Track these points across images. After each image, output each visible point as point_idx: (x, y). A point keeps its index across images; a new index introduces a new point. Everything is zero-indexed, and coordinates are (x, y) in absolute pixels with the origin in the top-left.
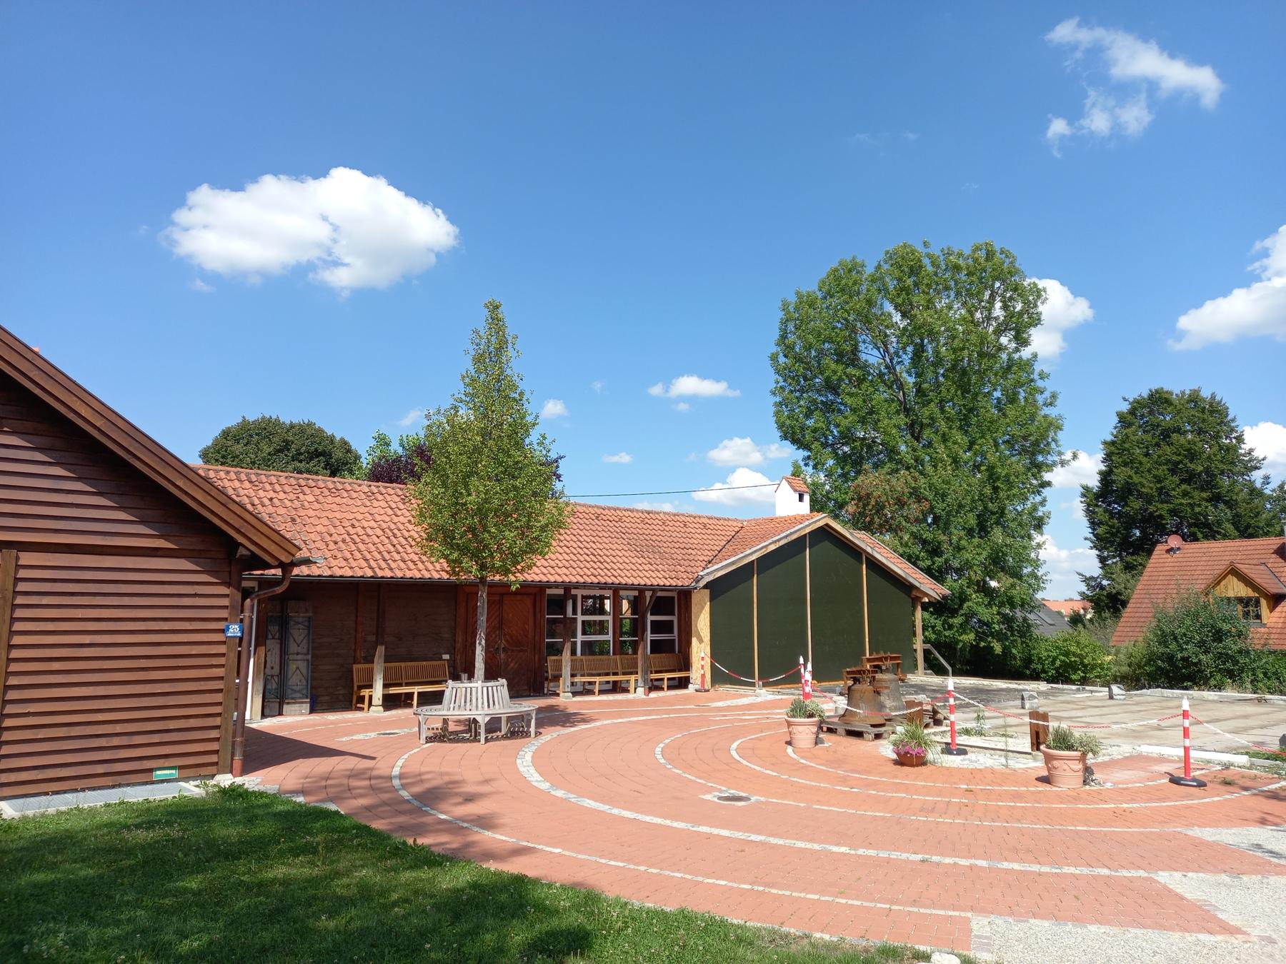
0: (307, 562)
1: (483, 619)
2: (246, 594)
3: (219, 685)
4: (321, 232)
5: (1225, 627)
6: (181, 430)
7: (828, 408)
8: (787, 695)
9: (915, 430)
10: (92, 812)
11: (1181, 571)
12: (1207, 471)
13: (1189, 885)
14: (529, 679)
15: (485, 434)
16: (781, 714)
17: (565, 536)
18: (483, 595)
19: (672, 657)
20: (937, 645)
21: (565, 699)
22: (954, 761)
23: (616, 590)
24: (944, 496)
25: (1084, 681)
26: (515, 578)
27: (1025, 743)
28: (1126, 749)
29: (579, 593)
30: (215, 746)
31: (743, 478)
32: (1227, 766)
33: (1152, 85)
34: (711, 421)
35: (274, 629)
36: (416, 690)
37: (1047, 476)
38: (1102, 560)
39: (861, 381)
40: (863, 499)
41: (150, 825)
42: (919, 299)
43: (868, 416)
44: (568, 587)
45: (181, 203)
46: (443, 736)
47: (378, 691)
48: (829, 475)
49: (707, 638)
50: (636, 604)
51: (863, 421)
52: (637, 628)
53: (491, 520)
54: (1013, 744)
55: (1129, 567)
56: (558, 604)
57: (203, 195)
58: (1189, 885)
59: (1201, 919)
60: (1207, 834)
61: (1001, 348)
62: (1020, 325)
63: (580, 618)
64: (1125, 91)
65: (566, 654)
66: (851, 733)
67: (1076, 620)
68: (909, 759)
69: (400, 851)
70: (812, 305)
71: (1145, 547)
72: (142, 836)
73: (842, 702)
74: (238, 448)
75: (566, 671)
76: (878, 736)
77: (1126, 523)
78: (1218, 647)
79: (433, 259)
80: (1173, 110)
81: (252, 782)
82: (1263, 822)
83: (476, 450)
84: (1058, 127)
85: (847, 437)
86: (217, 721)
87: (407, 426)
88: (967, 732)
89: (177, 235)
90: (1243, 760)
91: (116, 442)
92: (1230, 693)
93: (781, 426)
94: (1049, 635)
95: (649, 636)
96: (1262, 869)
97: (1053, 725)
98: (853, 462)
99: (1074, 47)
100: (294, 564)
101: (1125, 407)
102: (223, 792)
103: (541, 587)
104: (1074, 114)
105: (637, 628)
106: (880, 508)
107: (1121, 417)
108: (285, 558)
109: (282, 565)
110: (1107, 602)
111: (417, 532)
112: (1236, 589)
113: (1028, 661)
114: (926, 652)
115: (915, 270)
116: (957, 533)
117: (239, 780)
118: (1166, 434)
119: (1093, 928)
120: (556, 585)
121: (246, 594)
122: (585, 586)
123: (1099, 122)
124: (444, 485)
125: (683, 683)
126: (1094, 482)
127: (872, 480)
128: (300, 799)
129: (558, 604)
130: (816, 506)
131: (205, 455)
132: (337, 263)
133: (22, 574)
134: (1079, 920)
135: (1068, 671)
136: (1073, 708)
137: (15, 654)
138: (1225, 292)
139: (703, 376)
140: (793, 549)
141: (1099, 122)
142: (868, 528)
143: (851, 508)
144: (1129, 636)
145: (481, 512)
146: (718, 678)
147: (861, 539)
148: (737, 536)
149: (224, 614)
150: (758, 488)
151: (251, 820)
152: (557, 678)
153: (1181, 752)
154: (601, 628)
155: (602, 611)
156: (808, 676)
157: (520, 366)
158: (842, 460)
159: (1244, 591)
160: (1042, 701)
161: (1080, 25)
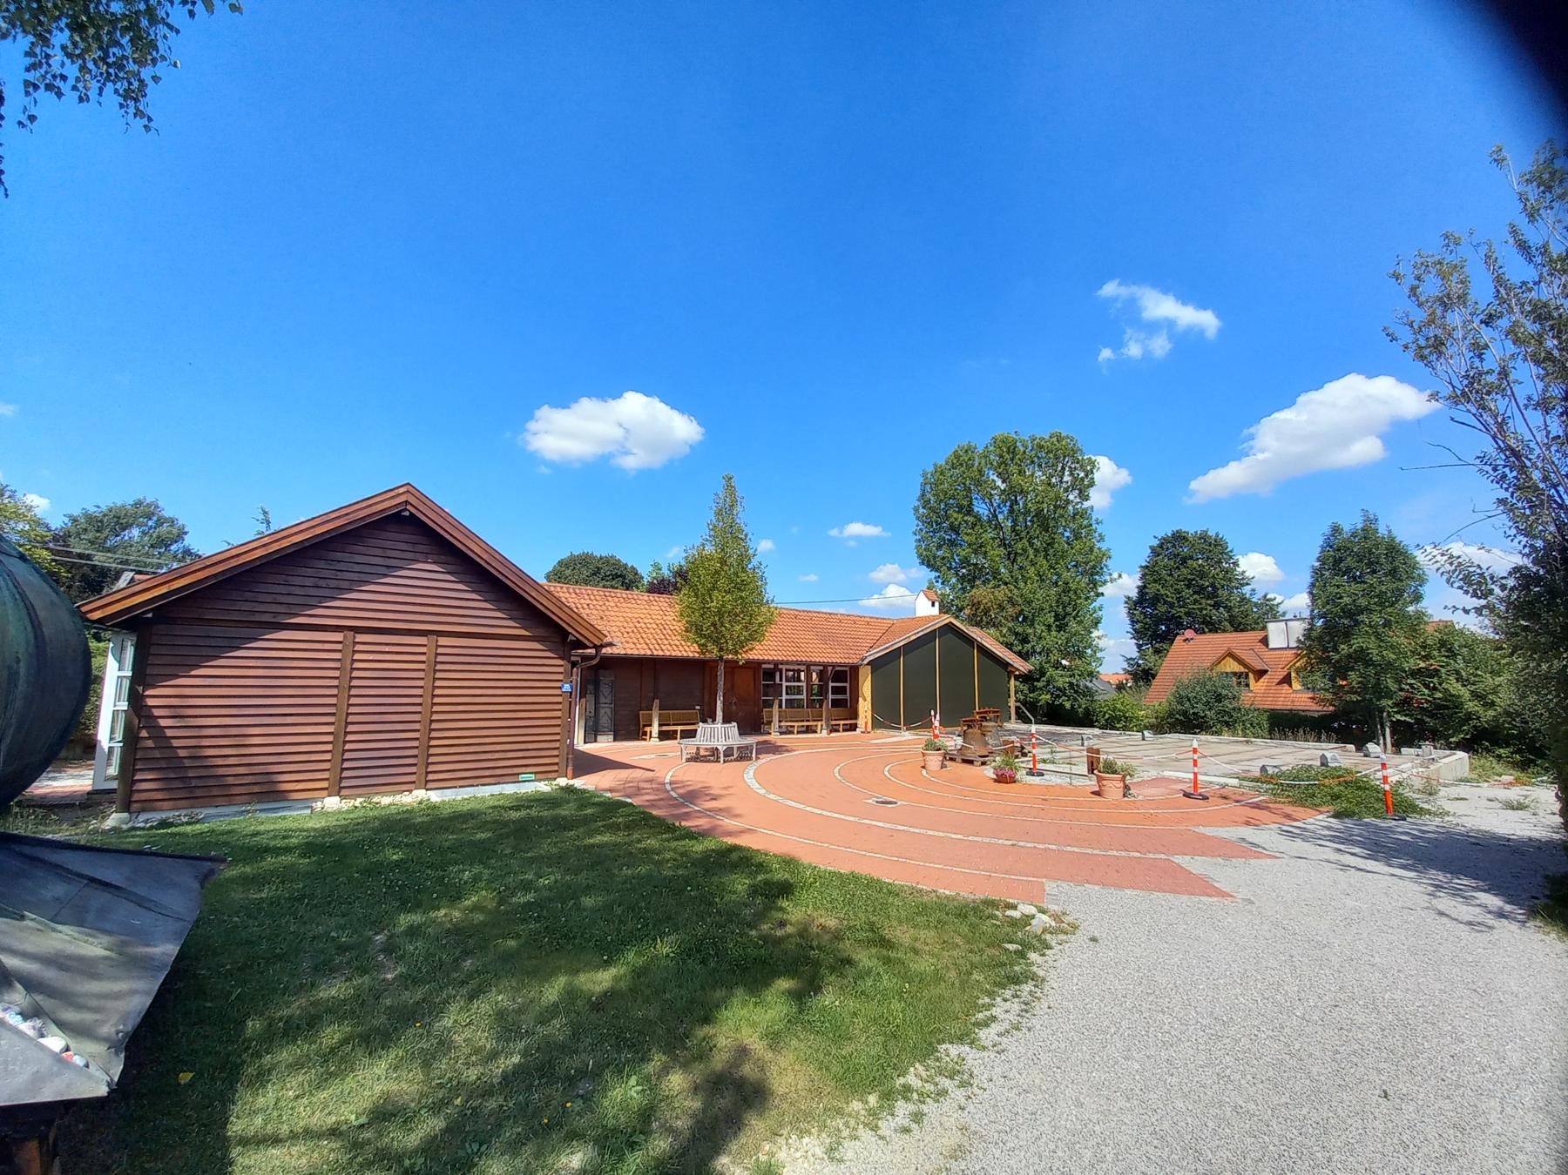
0: (610, 644)
1: (721, 683)
2: (574, 664)
3: (558, 722)
4: (618, 433)
5: (1224, 692)
6: (532, 557)
7: (952, 543)
8: (924, 736)
9: (1012, 557)
10: (483, 799)
11: (1193, 654)
12: (1213, 585)
13: (1195, 865)
14: (752, 724)
15: (723, 562)
16: (920, 748)
17: (773, 629)
18: (721, 667)
19: (846, 709)
20: (1025, 703)
21: (775, 737)
22: (1036, 780)
23: (809, 665)
24: (1030, 603)
25: (1125, 728)
26: (743, 657)
27: (1084, 769)
28: (1153, 773)
29: (784, 667)
30: (556, 760)
31: (892, 591)
32: (1224, 786)
33: (1170, 323)
34: (871, 553)
35: (591, 687)
36: (679, 728)
37: (1100, 590)
38: (1139, 646)
39: (974, 525)
40: (975, 605)
41: (517, 808)
42: (1013, 468)
43: (979, 548)
44: (776, 664)
45: (531, 417)
46: (696, 758)
47: (655, 729)
48: (953, 588)
49: (869, 699)
50: (821, 675)
51: (976, 552)
52: (822, 690)
53: (726, 619)
54: (1075, 770)
55: (1157, 651)
56: (770, 674)
57: (545, 411)
58: (1195, 865)
59: (1205, 887)
60: (1209, 831)
61: (1068, 502)
62: (1083, 487)
63: (785, 684)
64: (1153, 327)
65: (776, 707)
66: (965, 761)
67: (1120, 687)
68: (1003, 778)
69: (670, 829)
70: (942, 473)
71: (1168, 637)
72: (515, 815)
73: (960, 741)
74: (568, 572)
75: (776, 719)
76: (983, 763)
77: (1157, 621)
78: (1220, 706)
79: (688, 450)
80: (1187, 341)
81: (579, 783)
82: (1248, 823)
83: (717, 572)
84: (1106, 353)
85: (965, 562)
86: (557, 745)
87: (673, 557)
88: (1044, 761)
89: (529, 437)
90: (1235, 782)
91: (494, 568)
92: (1226, 737)
93: (920, 556)
94: (1105, 697)
95: (831, 697)
96: (1245, 854)
97: (1103, 757)
98: (970, 580)
99: (1115, 299)
100: (602, 646)
101: (1155, 543)
102: (562, 788)
103: (759, 663)
104: (1118, 345)
105: (822, 690)
106: (986, 612)
107: (1153, 549)
108: (597, 643)
109: (595, 647)
110: (1143, 676)
111: (679, 627)
112: (1231, 666)
113: (1087, 712)
114: (1017, 708)
115: (1012, 450)
116: (1039, 628)
117: (571, 782)
118: (1184, 560)
119: (1128, 891)
120: (768, 662)
121: (574, 664)
122: (787, 663)
123: (1134, 350)
124: (696, 595)
125: (853, 727)
126: (1134, 594)
127: (982, 593)
128: (609, 795)
129: (770, 674)
130: (944, 609)
131: (548, 577)
132: (628, 453)
133: (440, 650)
134: (1118, 886)
135: (1115, 721)
136: (1116, 746)
137: (436, 700)
138: (1224, 464)
139: (866, 522)
140: (928, 638)
141: (1134, 350)
142: (978, 624)
143: (967, 611)
144: (1157, 698)
145: (720, 613)
146: (876, 724)
147: (975, 633)
148: (890, 629)
149: (560, 677)
150: (906, 598)
151: (582, 807)
152: (769, 723)
153: (1191, 776)
154: (799, 690)
155: (799, 680)
156: (937, 723)
157: (745, 517)
158: (962, 579)
159: (1238, 668)
160: (1095, 741)
161: (1120, 284)
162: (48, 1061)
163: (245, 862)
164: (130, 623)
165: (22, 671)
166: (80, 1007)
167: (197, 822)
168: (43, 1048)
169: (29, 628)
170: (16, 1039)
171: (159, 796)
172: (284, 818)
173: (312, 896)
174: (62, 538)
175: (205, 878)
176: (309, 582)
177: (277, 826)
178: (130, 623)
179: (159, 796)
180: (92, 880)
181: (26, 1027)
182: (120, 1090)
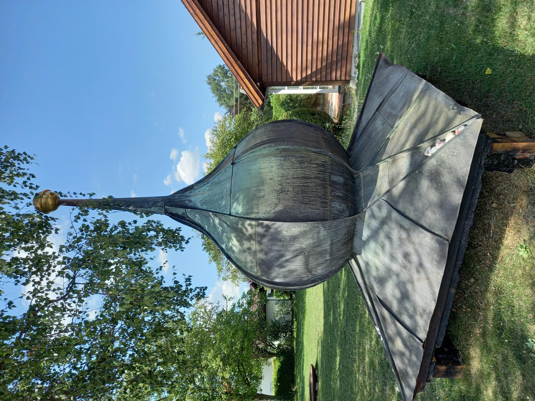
162: (458, 140)
163: (384, 38)
164: (263, 90)
165: (282, 147)
166: (436, 122)
167: (359, 54)
168: (450, 141)
169: (264, 146)
170: (442, 150)
171: (344, 70)
172: (364, 17)
173: (412, 6)
174: (230, 108)
175: (388, 63)
176: (232, 19)
177: (369, 21)
178: (263, 90)
179: (344, 70)
180: (377, 110)
181: (438, 146)
182: (482, 109)
